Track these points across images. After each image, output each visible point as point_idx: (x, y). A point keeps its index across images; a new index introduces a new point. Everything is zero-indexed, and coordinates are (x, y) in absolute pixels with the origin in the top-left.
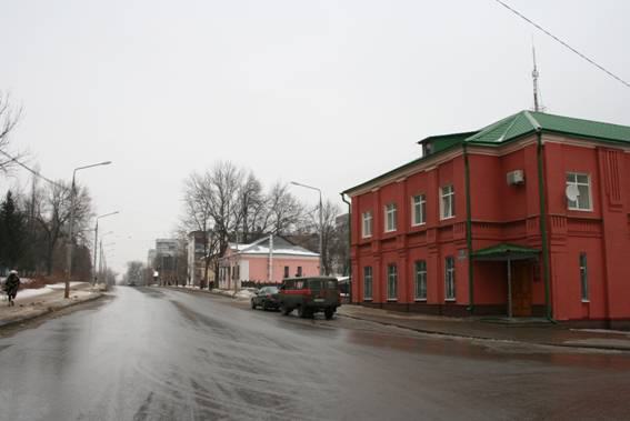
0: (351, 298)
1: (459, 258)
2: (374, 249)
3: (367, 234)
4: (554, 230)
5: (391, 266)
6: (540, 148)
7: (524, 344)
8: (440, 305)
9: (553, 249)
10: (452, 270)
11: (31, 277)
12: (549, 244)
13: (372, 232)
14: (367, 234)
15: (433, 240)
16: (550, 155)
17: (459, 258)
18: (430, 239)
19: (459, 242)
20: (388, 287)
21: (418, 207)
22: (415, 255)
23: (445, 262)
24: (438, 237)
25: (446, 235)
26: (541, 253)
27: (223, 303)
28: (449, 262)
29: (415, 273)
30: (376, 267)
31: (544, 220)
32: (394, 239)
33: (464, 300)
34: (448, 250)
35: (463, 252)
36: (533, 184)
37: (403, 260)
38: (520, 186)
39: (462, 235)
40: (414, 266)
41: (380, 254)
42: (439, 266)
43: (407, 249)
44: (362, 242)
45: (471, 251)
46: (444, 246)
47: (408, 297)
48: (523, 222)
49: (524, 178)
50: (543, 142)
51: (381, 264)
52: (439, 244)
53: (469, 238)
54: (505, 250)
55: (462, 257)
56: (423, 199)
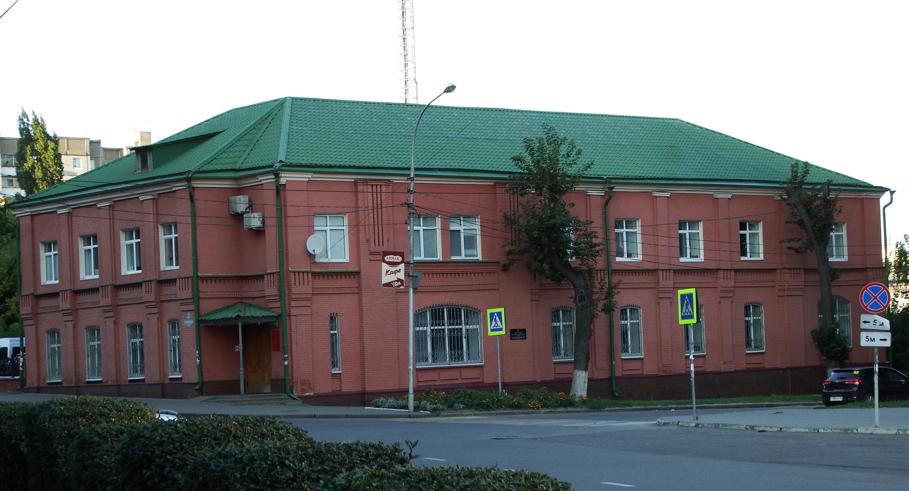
0: (23, 381)
1: (186, 322)
2: (64, 303)
3: (49, 277)
4: (296, 289)
5: (53, 332)
6: (280, 189)
7: (611, 424)
8: (163, 384)
9: (293, 311)
10: (176, 337)
11: (258, 478)
12: (290, 306)
13: (60, 277)
14: (88, 273)
15: (151, 297)
16: (291, 198)
17: (186, 322)
18: (148, 295)
19: (183, 302)
20: (88, 361)
21: (130, 247)
22: (129, 315)
23: (168, 328)
24: (159, 293)
25: (168, 291)
26: (279, 316)
27: (815, 409)
28: (174, 328)
29: (129, 341)
30: (67, 331)
31: (282, 277)
32: (95, 290)
33: (192, 377)
34: (171, 311)
35: (189, 315)
36: (271, 233)
37: (110, 322)
38: (259, 232)
39: (187, 294)
40: (127, 331)
41: (74, 311)
42: (161, 334)
43: (115, 307)
44: (41, 291)
45: (199, 314)
46: (121, 307)
47: (118, 371)
48: (261, 277)
49: (263, 222)
50: (283, 181)
51: (160, 319)
52: (160, 303)
53: (196, 298)
54: (234, 316)
55: (189, 322)
56: (138, 237)
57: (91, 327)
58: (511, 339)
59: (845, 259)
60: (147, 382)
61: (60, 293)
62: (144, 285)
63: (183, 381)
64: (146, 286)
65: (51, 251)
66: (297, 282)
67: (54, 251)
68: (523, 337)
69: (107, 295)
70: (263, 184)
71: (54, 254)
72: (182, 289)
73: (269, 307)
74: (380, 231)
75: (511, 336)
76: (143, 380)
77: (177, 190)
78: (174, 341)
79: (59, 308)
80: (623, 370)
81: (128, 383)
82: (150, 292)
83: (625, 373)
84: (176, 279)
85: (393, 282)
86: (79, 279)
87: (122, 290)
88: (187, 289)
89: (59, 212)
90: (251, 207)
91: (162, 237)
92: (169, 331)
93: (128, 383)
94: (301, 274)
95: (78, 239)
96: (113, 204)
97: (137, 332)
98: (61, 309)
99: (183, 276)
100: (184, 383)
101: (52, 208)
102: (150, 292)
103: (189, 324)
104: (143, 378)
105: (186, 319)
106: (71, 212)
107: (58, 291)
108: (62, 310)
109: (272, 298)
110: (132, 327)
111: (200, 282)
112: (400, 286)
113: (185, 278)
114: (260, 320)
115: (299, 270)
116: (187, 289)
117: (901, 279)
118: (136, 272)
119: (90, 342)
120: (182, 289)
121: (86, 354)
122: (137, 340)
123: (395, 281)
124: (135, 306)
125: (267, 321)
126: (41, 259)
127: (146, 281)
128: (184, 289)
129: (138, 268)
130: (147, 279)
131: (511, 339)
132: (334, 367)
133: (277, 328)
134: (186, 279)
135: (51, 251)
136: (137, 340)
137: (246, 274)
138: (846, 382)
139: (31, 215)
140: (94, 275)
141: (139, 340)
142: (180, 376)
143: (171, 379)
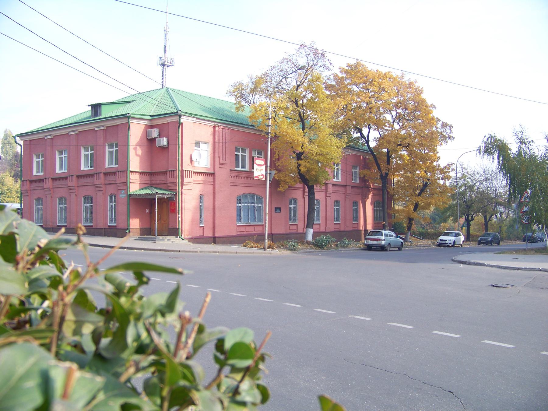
1: (120, 196)
40: (58, 201)
57: (60, 197)
58: (275, 212)
59: (340, 180)
60: (94, 227)
61: (45, 179)
62: (95, 175)
63: (117, 228)
64: (97, 175)
65: (63, 155)
66: (171, 176)
67: (64, 155)
68: (280, 212)
69: (72, 180)
70: (168, 123)
71: (64, 157)
72: (120, 177)
73: (169, 189)
74: (225, 148)
75: (275, 211)
76: (92, 226)
77: (119, 124)
78: (112, 206)
79: (67, 185)
80: (246, 231)
81: (108, 228)
82: (99, 179)
83: (239, 233)
84: (116, 172)
85: (259, 176)
86: (33, 175)
87: (81, 178)
88: (123, 177)
89: (46, 138)
90: (160, 135)
91: (107, 150)
92: (35, 204)
93: (108, 228)
94: (171, 172)
95: (81, 148)
96: (78, 133)
97: (63, 201)
98: (44, 188)
99: (120, 170)
100: (94, 228)
101: (93, 127)
102: (99, 179)
103: (123, 197)
104: (92, 225)
105: (121, 194)
106: (52, 138)
107: (43, 178)
108: (45, 188)
109: (171, 184)
110: (86, 198)
111: (131, 173)
112: (262, 178)
113: (122, 171)
114: (166, 196)
115: (188, 170)
116: (123, 177)
117: (546, 184)
118: (89, 168)
119: (37, 206)
120: (120, 177)
121: (108, 210)
122: (89, 205)
123: (260, 175)
124: (89, 186)
125: (170, 196)
126: (34, 162)
127: (97, 173)
128: (121, 178)
129: (91, 167)
130: (97, 172)
131: (275, 212)
132: (201, 223)
133: (174, 200)
134: (123, 172)
135: (40, 158)
136: (63, 205)
137: (154, 171)
138: (450, 245)
139: (30, 140)
140: (64, 170)
141: (64, 206)
142: (115, 225)
143: (109, 226)
